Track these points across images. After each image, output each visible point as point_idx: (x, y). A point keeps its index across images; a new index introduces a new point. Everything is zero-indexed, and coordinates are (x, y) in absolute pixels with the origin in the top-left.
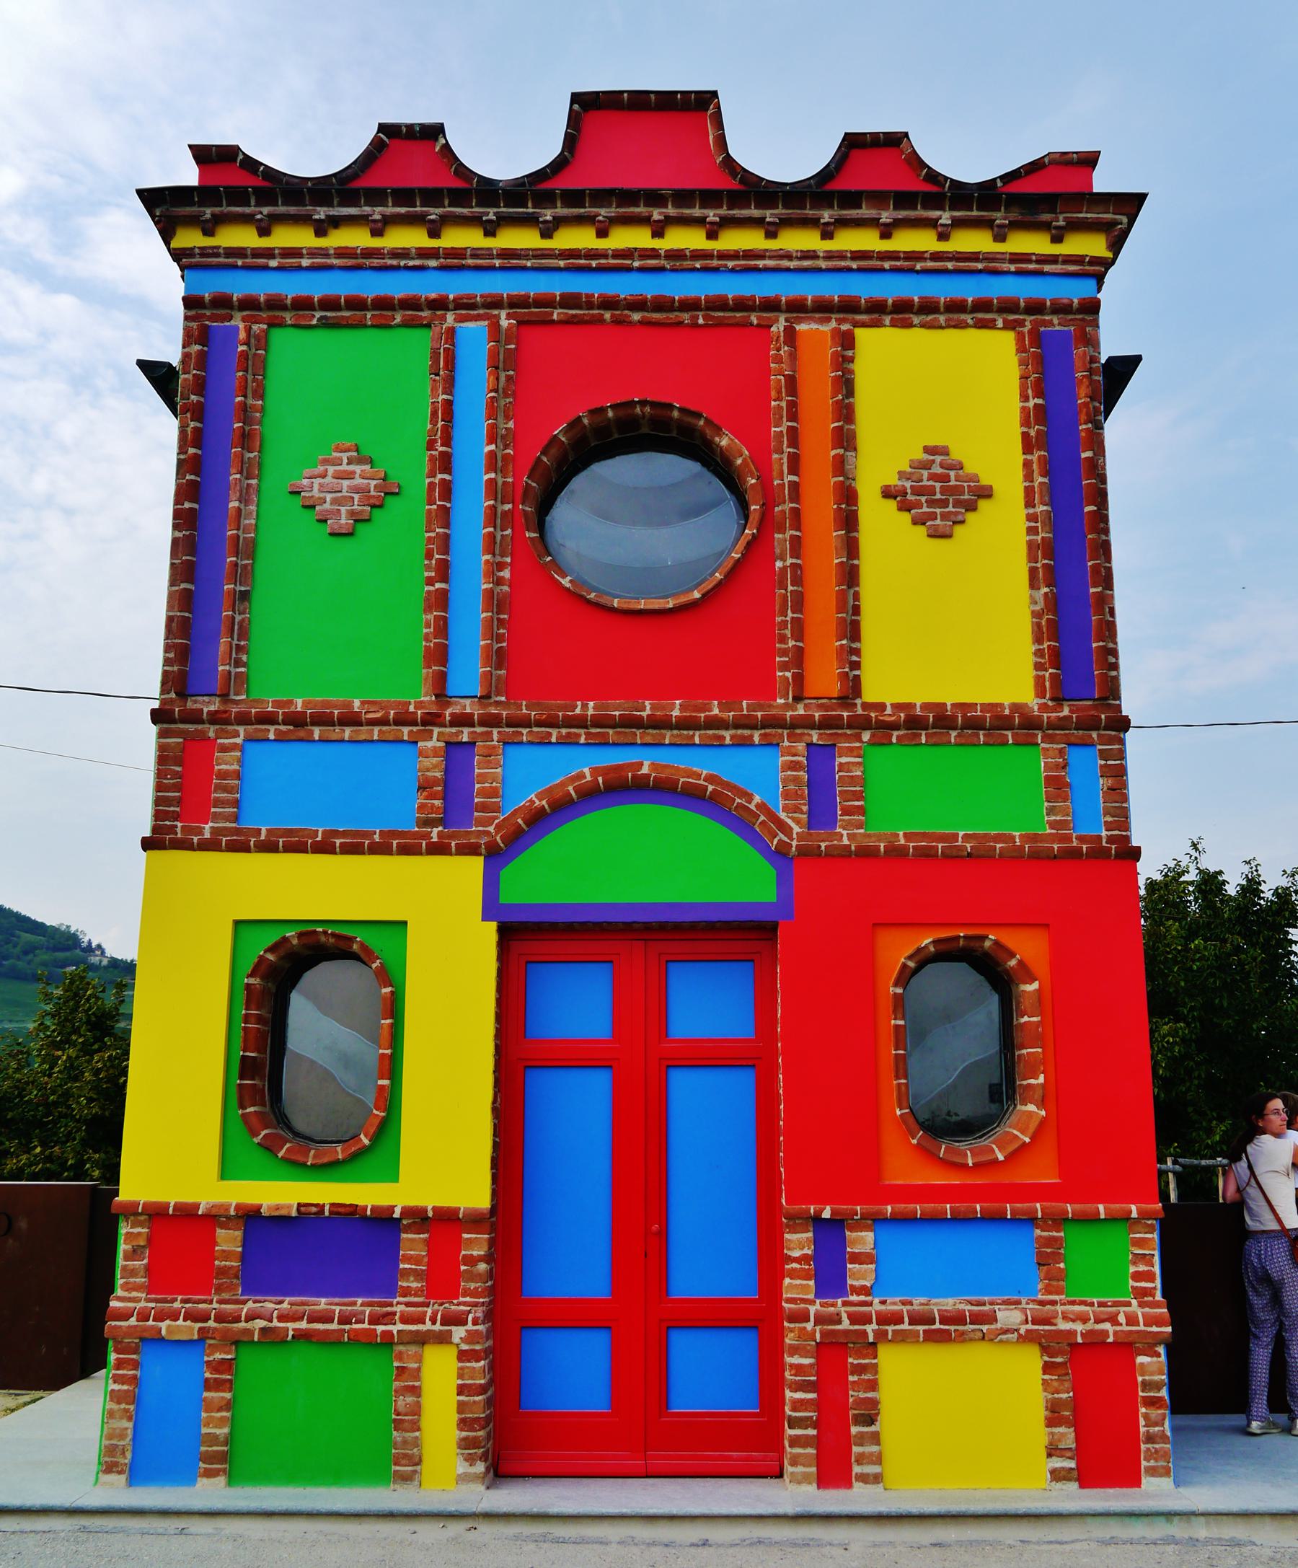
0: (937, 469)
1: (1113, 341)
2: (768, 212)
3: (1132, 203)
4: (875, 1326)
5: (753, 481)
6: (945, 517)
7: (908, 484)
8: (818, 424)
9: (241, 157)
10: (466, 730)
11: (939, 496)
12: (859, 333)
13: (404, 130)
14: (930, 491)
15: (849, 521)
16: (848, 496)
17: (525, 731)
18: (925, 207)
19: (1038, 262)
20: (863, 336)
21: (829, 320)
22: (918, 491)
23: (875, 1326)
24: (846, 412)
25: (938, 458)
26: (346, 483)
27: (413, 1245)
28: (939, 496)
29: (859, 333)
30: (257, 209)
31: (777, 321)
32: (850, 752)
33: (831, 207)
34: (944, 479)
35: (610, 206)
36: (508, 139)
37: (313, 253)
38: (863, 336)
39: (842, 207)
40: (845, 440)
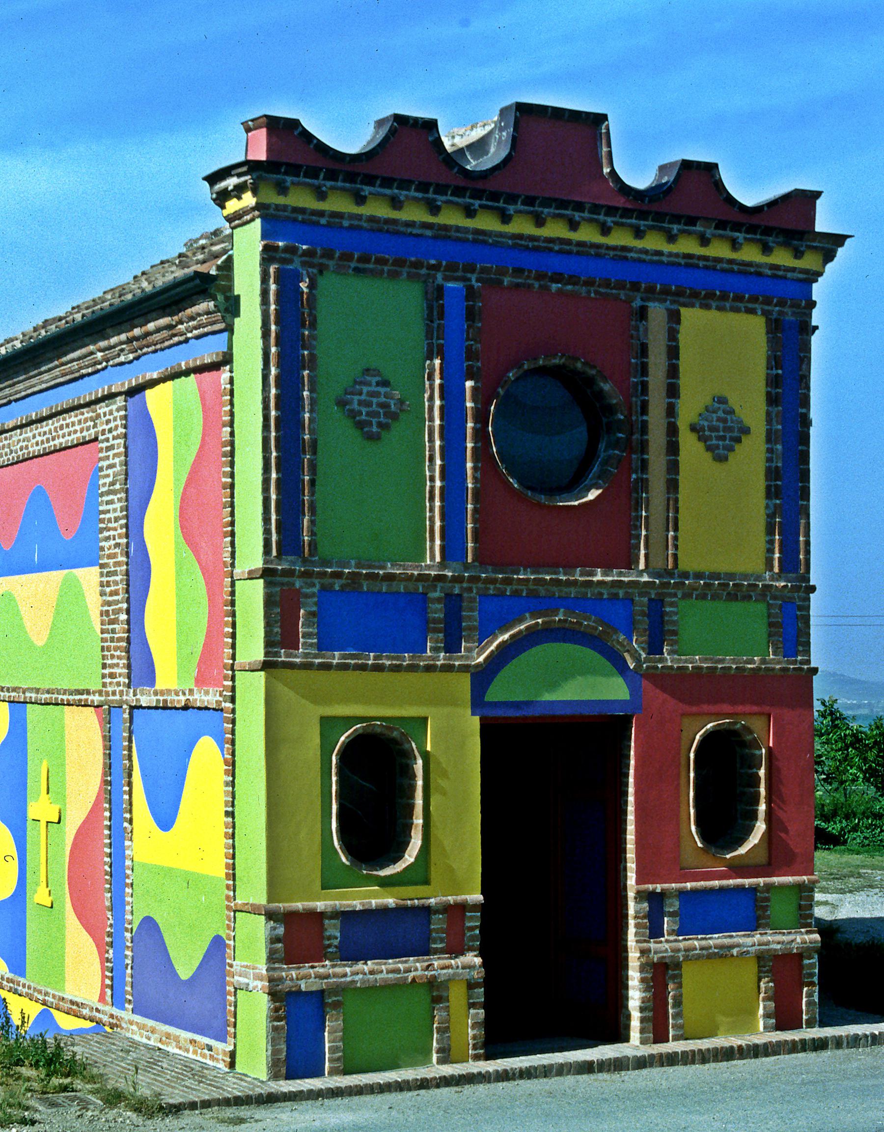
0: (721, 414)
1: (814, 323)
2: (642, 222)
3: (839, 240)
4: (683, 953)
5: (622, 417)
6: (725, 448)
7: (706, 424)
8: (657, 377)
9: (300, 129)
10: (457, 586)
11: (721, 434)
12: (683, 310)
13: (411, 122)
14: (716, 429)
15: (673, 448)
16: (672, 430)
17: (492, 587)
18: (732, 230)
19: (784, 271)
20: (686, 313)
21: (665, 301)
22: (712, 429)
23: (683, 953)
24: (673, 371)
25: (722, 406)
26: (375, 400)
27: (438, 922)
28: (721, 434)
29: (683, 310)
30: (323, 182)
31: (635, 299)
32: (672, 604)
33: (679, 223)
34: (725, 421)
35: (550, 207)
36: (468, 128)
37: (352, 216)
38: (686, 313)
39: (686, 224)
40: (673, 391)
